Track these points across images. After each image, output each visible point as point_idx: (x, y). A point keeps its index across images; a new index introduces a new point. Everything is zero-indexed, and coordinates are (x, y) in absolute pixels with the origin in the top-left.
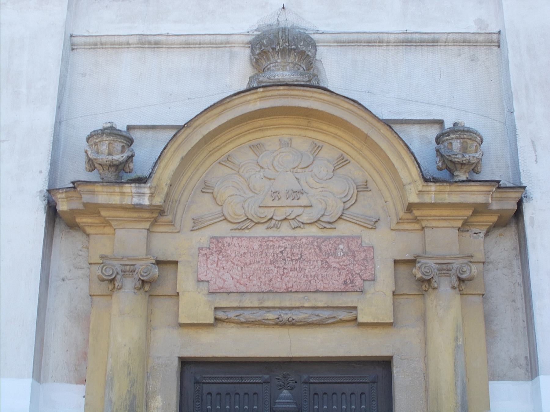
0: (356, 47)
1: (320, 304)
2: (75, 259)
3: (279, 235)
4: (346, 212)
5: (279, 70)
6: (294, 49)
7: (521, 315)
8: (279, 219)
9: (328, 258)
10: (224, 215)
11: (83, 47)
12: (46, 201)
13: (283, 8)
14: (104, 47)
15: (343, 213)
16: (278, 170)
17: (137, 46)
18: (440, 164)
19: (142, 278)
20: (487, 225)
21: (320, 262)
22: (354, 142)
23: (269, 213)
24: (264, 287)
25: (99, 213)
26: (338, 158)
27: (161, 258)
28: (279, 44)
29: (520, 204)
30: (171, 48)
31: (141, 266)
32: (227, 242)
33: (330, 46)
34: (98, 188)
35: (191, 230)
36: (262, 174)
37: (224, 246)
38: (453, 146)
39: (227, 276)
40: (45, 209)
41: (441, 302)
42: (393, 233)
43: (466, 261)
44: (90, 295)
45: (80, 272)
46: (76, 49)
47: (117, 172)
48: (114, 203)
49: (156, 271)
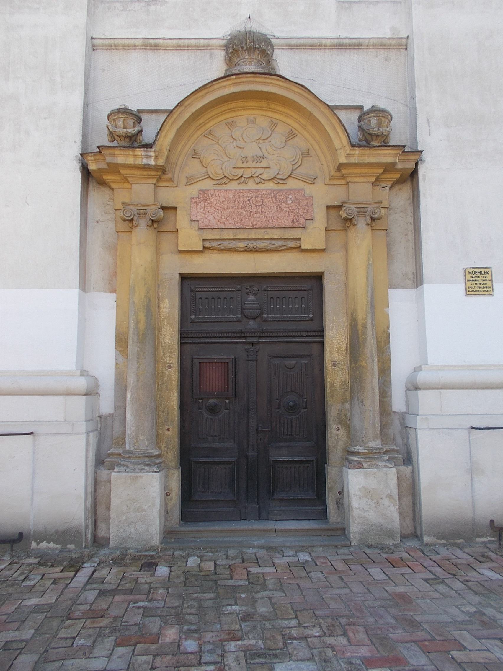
0: (303, 50)
1: (275, 237)
2: (105, 207)
3: (247, 188)
4: (293, 172)
5: (246, 65)
6: (258, 48)
7: (411, 245)
8: (247, 177)
9: (281, 204)
10: (208, 174)
11: (101, 48)
12: (81, 164)
13: (249, 17)
14: (117, 48)
15: (292, 173)
16: (246, 141)
17: (142, 48)
18: (361, 137)
19: (152, 218)
20: (391, 181)
21: (275, 207)
22: (301, 120)
23: (240, 172)
24: (237, 224)
25: (119, 172)
26: (289, 132)
27: (165, 205)
28: (246, 43)
29: (417, 164)
30: (167, 50)
31: (151, 210)
32: (210, 194)
33: (283, 49)
34: (117, 152)
35: (185, 185)
36: (234, 144)
37: (208, 196)
38: (372, 123)
39: (211, 217)
40: (80, 169)
41: (358, 234)
42: (327, 187)
43: (377, 205)
44: (117, 232)
45: (109, 217)
46: (97, 49)
47: (131, 142)
48: (129, 163)
49: (161, 213)
